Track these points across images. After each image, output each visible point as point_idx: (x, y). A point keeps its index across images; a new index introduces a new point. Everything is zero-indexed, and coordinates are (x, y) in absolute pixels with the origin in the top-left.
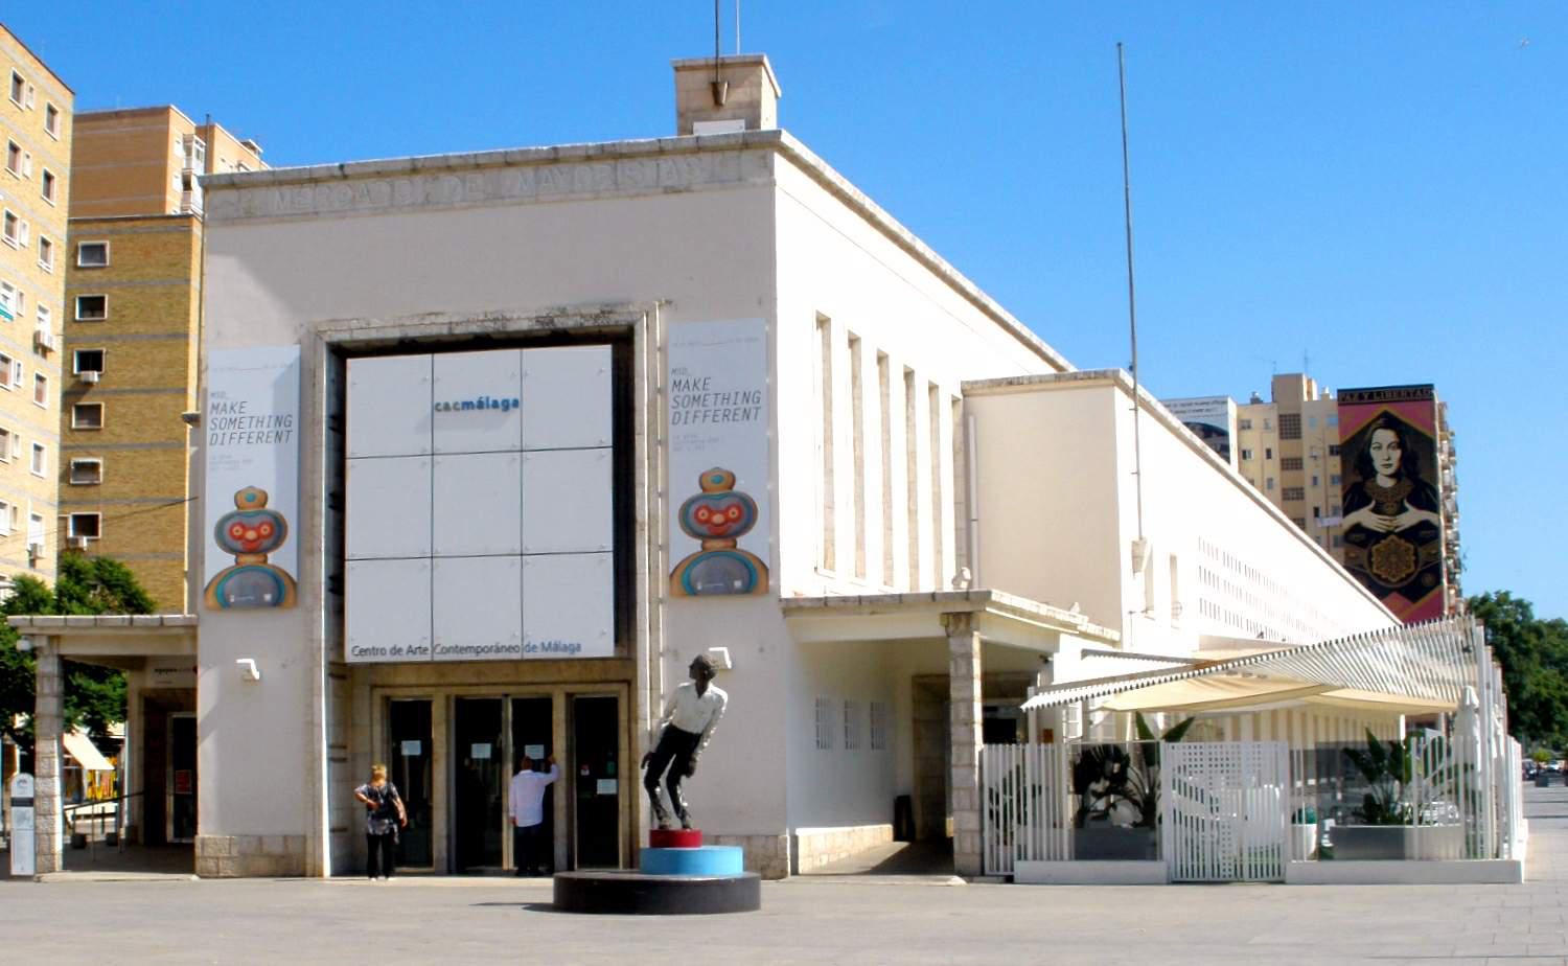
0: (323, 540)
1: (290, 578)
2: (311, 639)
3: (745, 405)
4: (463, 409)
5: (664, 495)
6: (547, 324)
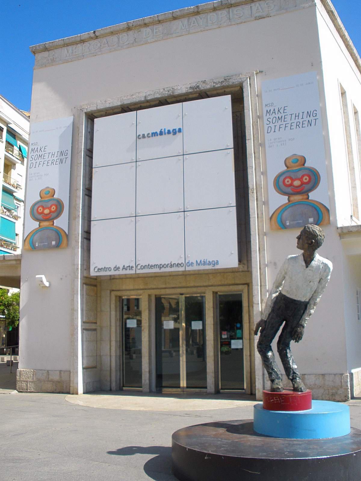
0: (81, 211)
1: (65, 233)
2: (74, 264)
3: (310, 119)
4: (152, 136)
5: (264, 173)
6: (196, 88)
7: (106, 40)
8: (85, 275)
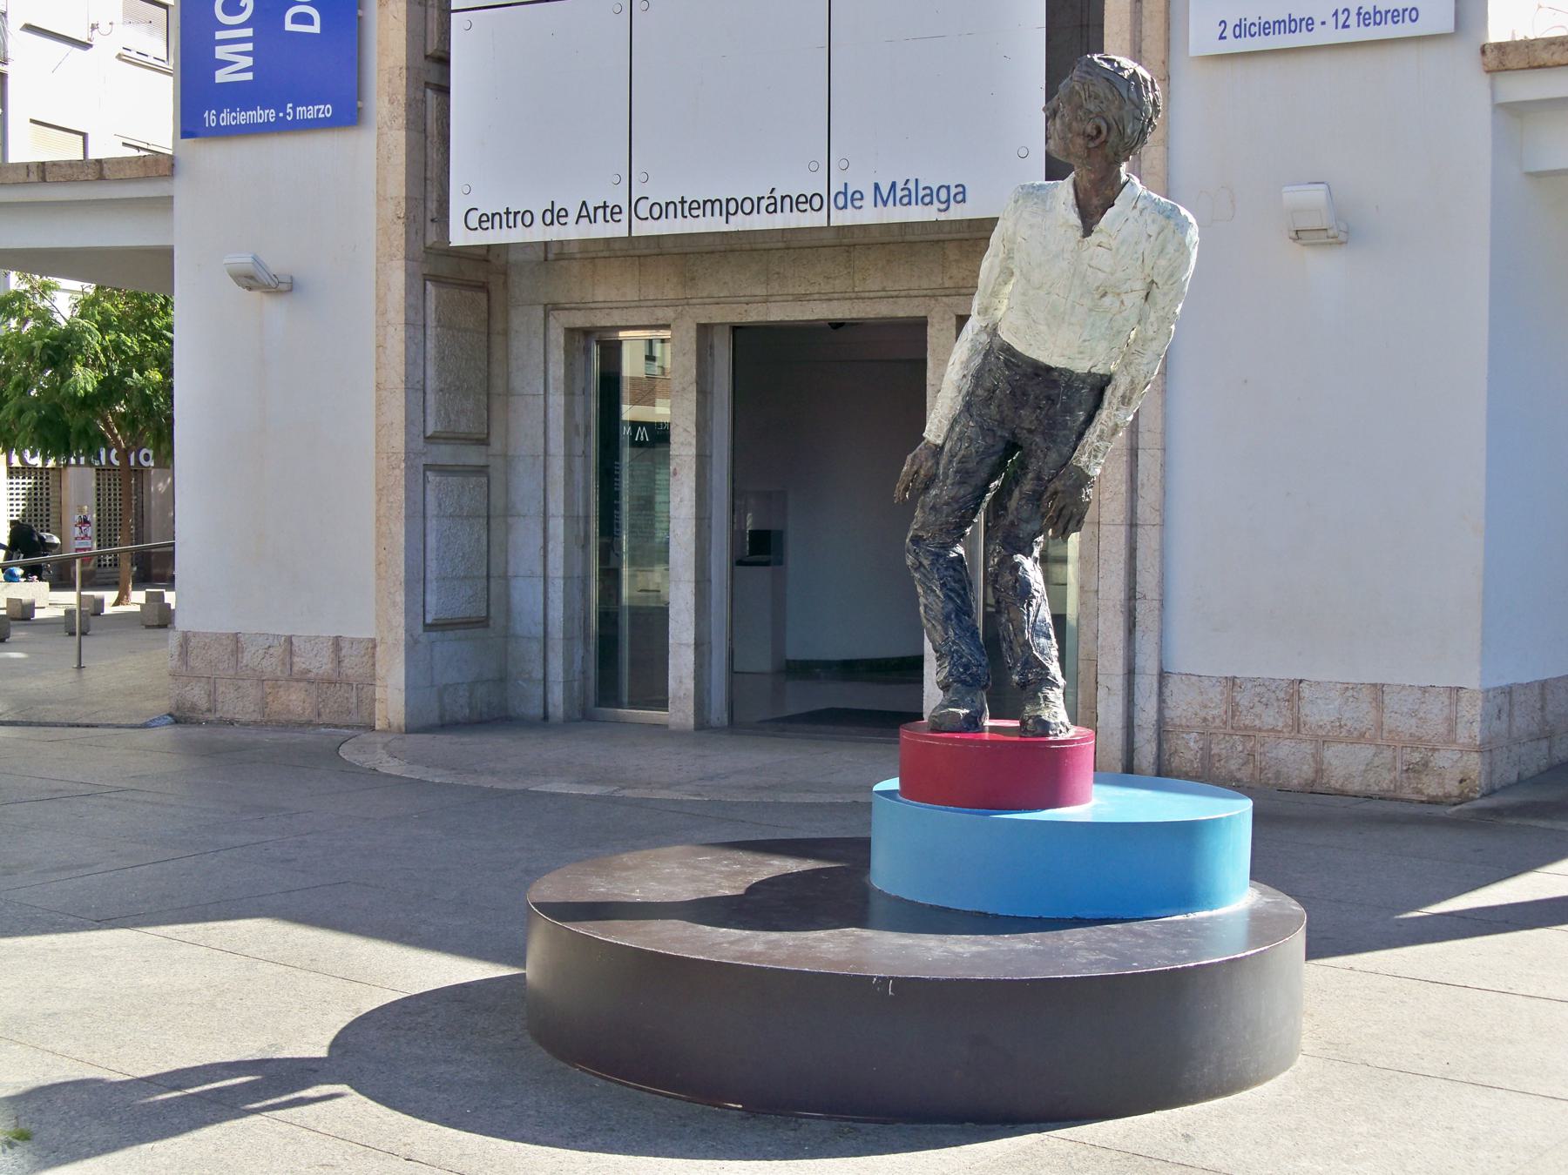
8: (432, 238)
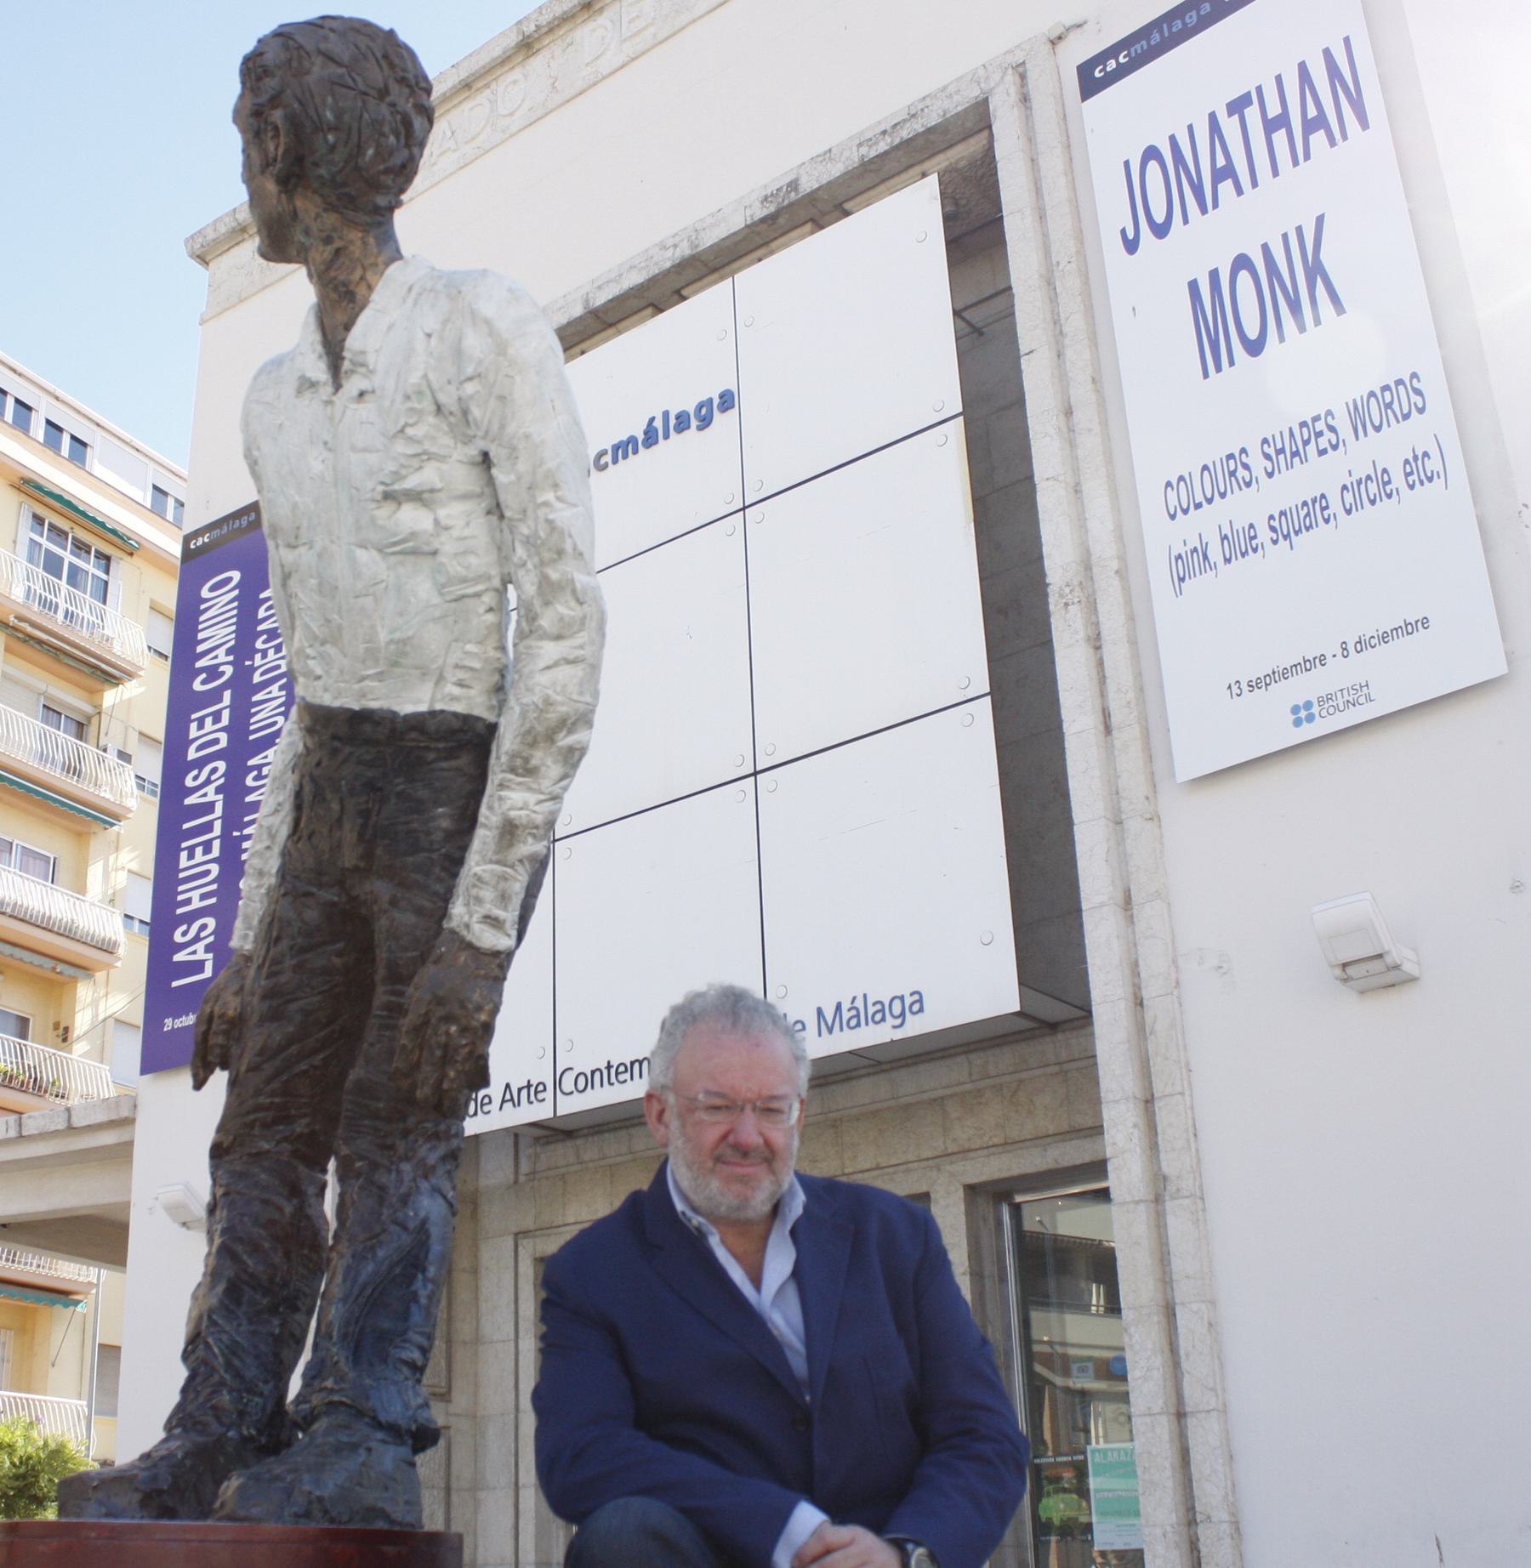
7: (449, 123)
